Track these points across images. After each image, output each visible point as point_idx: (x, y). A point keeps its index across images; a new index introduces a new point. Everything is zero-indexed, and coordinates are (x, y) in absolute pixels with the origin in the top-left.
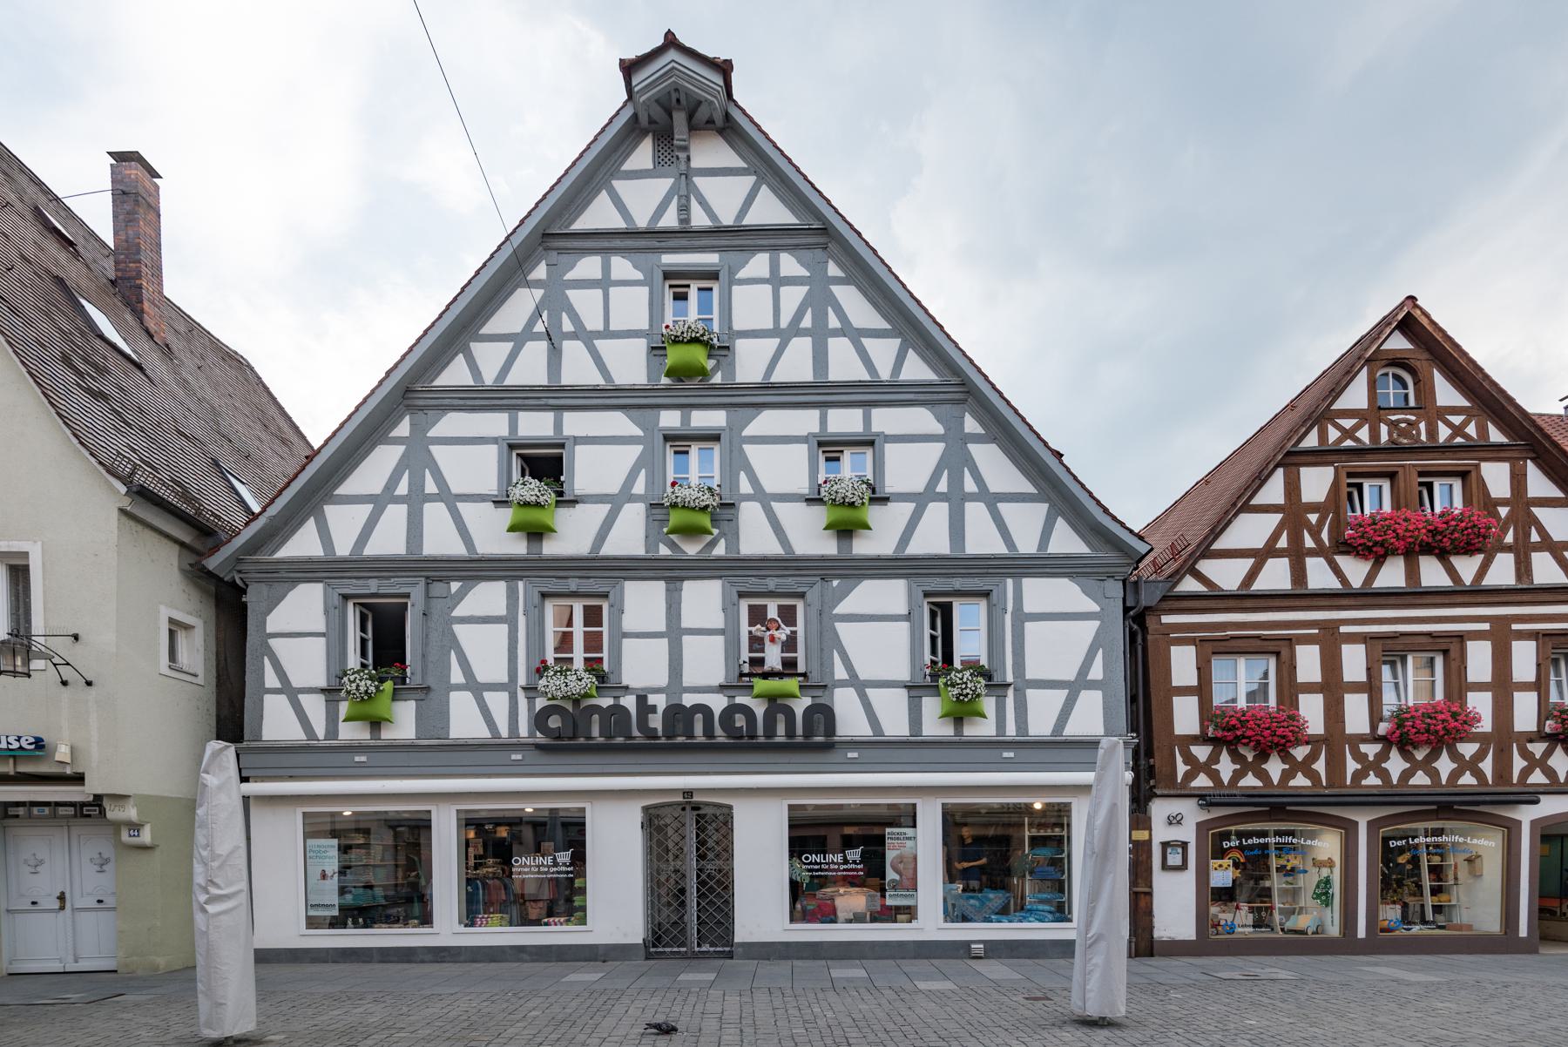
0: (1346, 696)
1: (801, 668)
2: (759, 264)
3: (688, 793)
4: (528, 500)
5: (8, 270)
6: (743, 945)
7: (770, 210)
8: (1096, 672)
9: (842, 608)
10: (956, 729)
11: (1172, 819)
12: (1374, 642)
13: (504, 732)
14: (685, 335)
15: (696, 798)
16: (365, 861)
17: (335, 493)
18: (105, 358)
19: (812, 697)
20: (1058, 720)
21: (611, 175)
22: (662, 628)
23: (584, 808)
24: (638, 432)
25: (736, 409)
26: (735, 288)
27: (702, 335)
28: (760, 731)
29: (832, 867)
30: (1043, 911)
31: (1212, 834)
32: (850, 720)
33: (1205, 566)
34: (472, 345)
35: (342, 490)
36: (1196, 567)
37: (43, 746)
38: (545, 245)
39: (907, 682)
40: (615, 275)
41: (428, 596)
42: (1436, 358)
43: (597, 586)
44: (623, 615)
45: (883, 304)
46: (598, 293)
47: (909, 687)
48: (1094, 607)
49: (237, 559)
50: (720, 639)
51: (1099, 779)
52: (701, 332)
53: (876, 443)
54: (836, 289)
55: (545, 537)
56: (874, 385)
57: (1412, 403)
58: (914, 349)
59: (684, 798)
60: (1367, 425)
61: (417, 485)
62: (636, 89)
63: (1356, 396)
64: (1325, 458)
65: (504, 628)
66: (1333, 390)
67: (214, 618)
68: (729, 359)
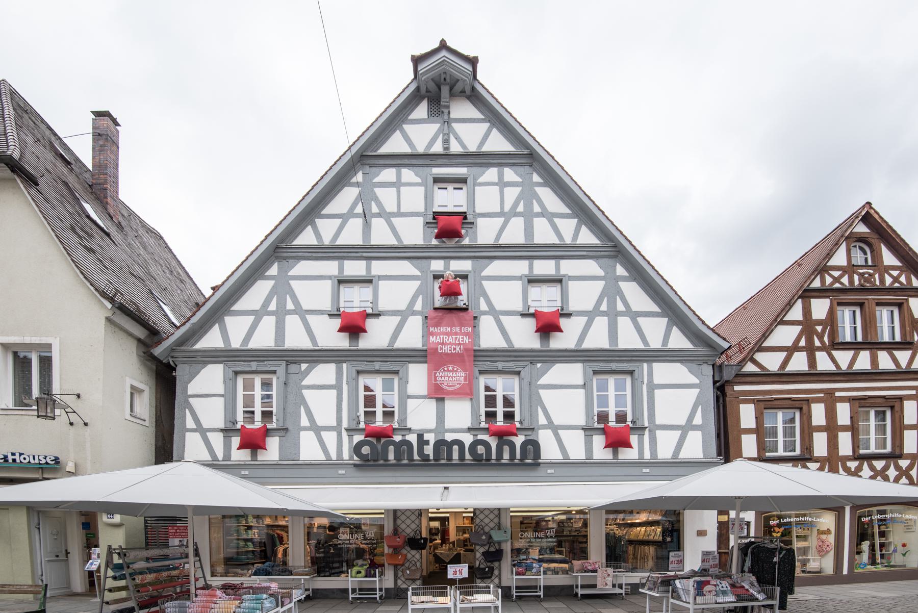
0: (839, 433)
2: (491, 174)
5: (41, 177)
7: (498, 143)
9: (543, 381)
10: (614, 455)
12: (854, 401)
13: (334, 456)
17: (231, 309)
18: (91, 229)
19: (525, 435)
21: (403, 121)
24: (418, 273)
25: (478, 260)
26: (477, 188)
28: (494, 457)
31: (764, 516)
32: (549, 451)
33: (759, 357)
34: (316, 220)
36: (754, 357)
37: (59, 462)
38: (361, 162)
39: (584, 426)
40: (404, 180)
41: (287, 373)
42: (882, 238)
43: (392, 367)
44: (408, 385)
45: (566, 198)
46: (394, 190)
48: (696, 381)
49: (172, 349)
53: (564, 281)
57: (870, 263)
58: (585, 225)
60: (847, 275)
61: (281, 304)
62: (420, 72)
63: (840, 258)
64: (824, 294)
65: (334, 392)
66: (828, 254)
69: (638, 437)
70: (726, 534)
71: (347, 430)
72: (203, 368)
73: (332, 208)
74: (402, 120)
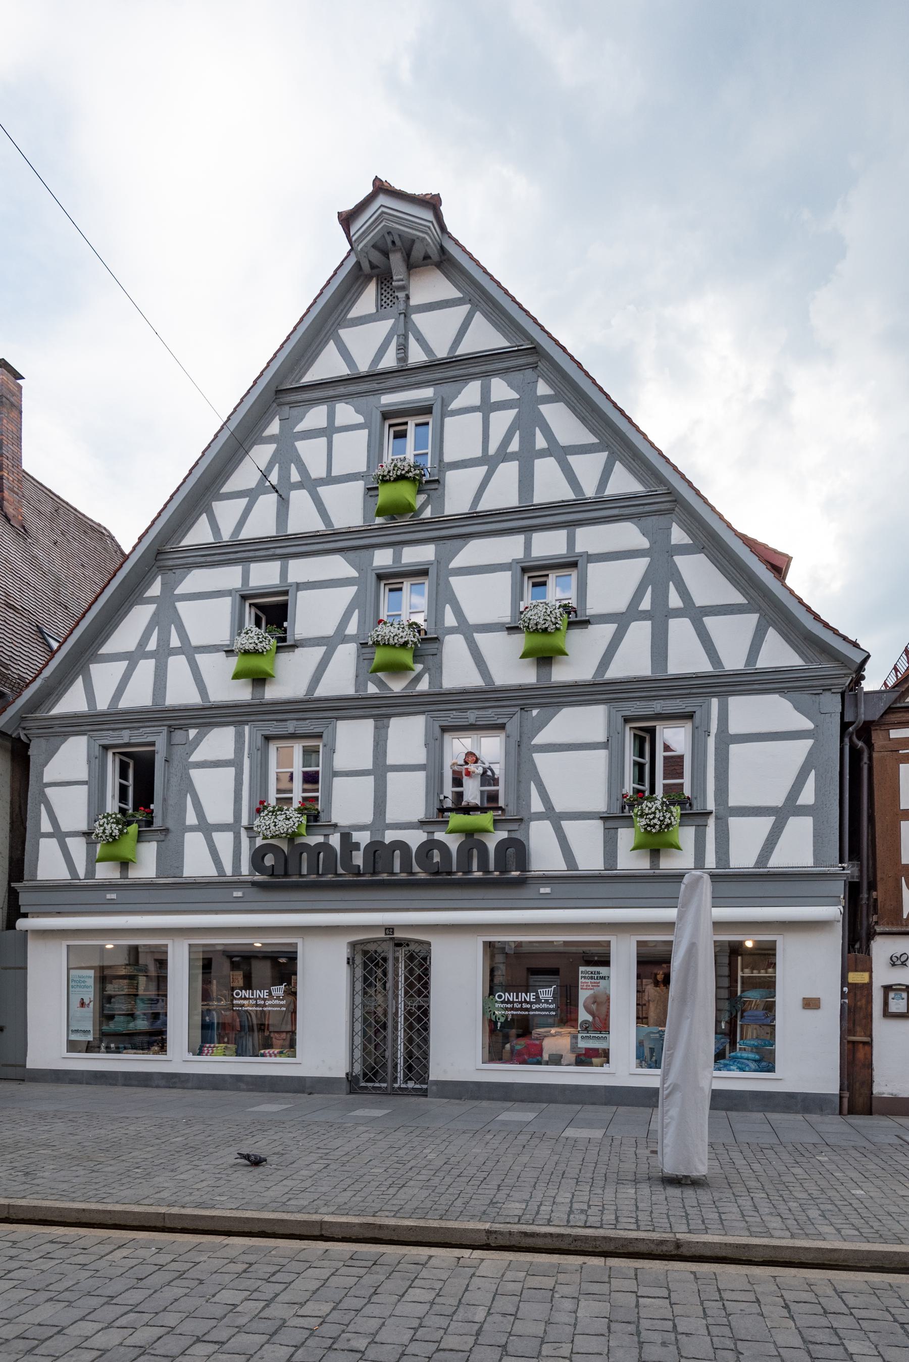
1: (501, 803)
2: (470, 394)
3: (390, 929)
4: (247, 648)
6: (437, 1083)
8: (807, 796)
10: (652, 862)
11: (894, 959)
13: (228, 870)
14: (391, 474)
15: (398, 935)
16: (126, 990)
19: (509, 831)
20: (762, 850)
22: (369, 765)
23: (609, 942)
24: (354, 573)
27: (408, 472)
29: (525, 1006)
30: (748, 1059)
35: (105, 650)
39: (604, 813)
43: (312, 727)
49: (21, 718)
50: (421, 775)
51: (681, 916)
52: (406, 469)
54: (544, 409)
55: (267, 682)
56: (580, 504)
59: (386, 934)
61: (164, 640)
65: (231, 771)
67: (9, 770)
68: (439, 492)
69: (696, 830)
70: (866, 1009)
72: (63, 743)
73: (232, 484)
74: (337, 322)
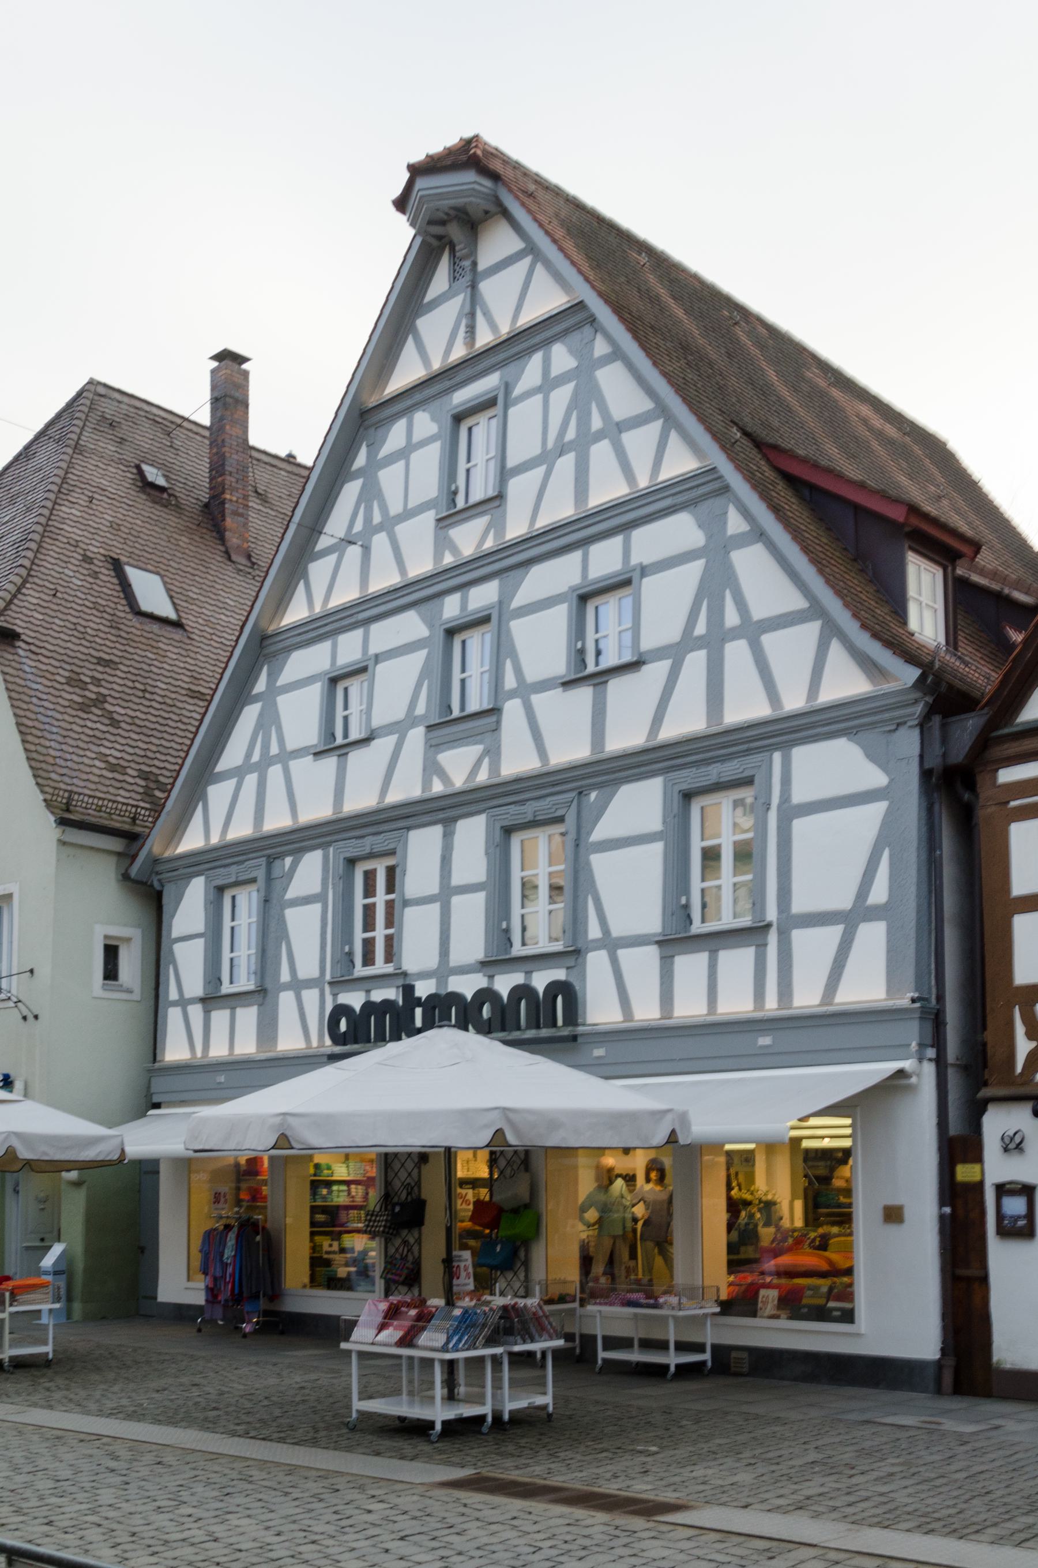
19: (568, 968)
47: (659, 943)
57: (206, 704)
71: (330, 983)
